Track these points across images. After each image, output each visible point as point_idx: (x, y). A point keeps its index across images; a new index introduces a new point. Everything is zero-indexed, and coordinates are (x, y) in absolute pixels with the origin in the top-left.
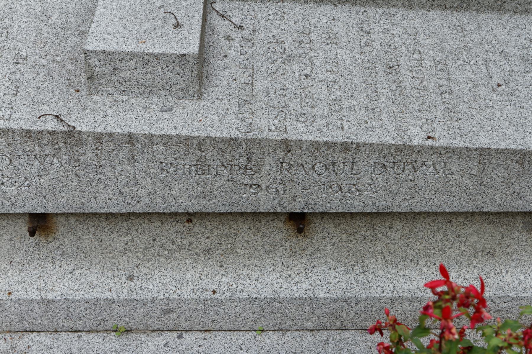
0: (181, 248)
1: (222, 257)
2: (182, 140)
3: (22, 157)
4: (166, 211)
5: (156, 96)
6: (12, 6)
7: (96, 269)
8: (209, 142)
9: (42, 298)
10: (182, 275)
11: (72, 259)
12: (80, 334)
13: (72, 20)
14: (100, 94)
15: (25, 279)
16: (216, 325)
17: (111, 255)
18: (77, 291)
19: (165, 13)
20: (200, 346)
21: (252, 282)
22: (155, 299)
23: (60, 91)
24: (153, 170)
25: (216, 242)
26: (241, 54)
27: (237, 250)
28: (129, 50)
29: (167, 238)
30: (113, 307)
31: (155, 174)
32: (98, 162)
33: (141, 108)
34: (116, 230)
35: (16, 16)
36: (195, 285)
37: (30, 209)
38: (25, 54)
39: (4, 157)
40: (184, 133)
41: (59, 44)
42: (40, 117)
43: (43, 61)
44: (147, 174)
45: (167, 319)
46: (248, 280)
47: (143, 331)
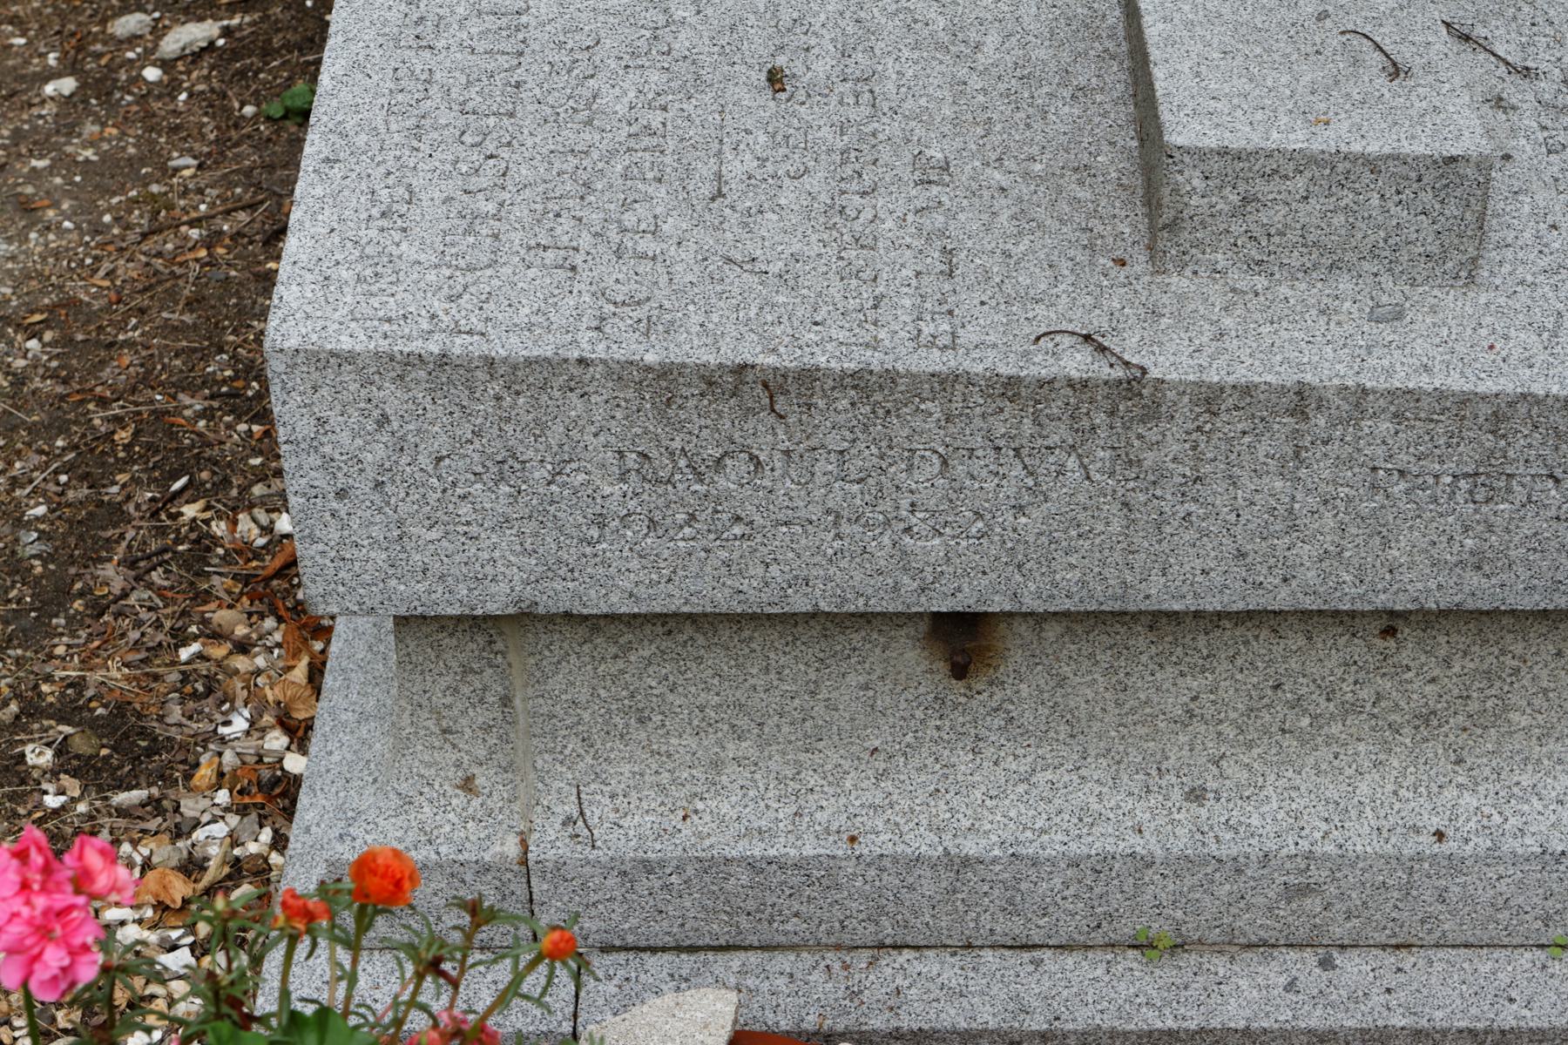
0: (1355, 708)
1: (1465, 736)
2: (1448, 404)
3: (980, 453)
4: (1358, 606)
5: (1347, 277)
6: (862, 14)
7: (1097, 769)
8: (1524, 410)
9: (946, 852)
10: (1344, 787)
11: (1032, 741)
12: (1037, 954)
13: (1042, 53)
14: (1188, 272)
15: (895, 797)
16: (1430, 932)
17: (1142, 730)
18: (1043, 831)
19: (1343, 33)
20: (1388, 991)
21: (1546, 807)
22: (1271, 856)
23: (1070, 264)
24: (1347, 490)
25: (1456, 692)
26: (1549, 152)
27: (1511, 715)
28: (1297, 146)
29: (1314, 681)
30: (1147, 879)
31: (1349, 500)
32: (1195, 468)
33: (1314, 312)
34: (1174, 659)
35: (881, 44)
36: (1382, 815)
37: (971, 602)
38: (939, 156)
39: (928, 453)
40: (1456, 383)
41: (1028, 126)
42: (1038, 339)
43: (997, 175)
44: (1326, 502)
45: (1293, 912)
46: (1534, 800)
47: (1218, 948)
